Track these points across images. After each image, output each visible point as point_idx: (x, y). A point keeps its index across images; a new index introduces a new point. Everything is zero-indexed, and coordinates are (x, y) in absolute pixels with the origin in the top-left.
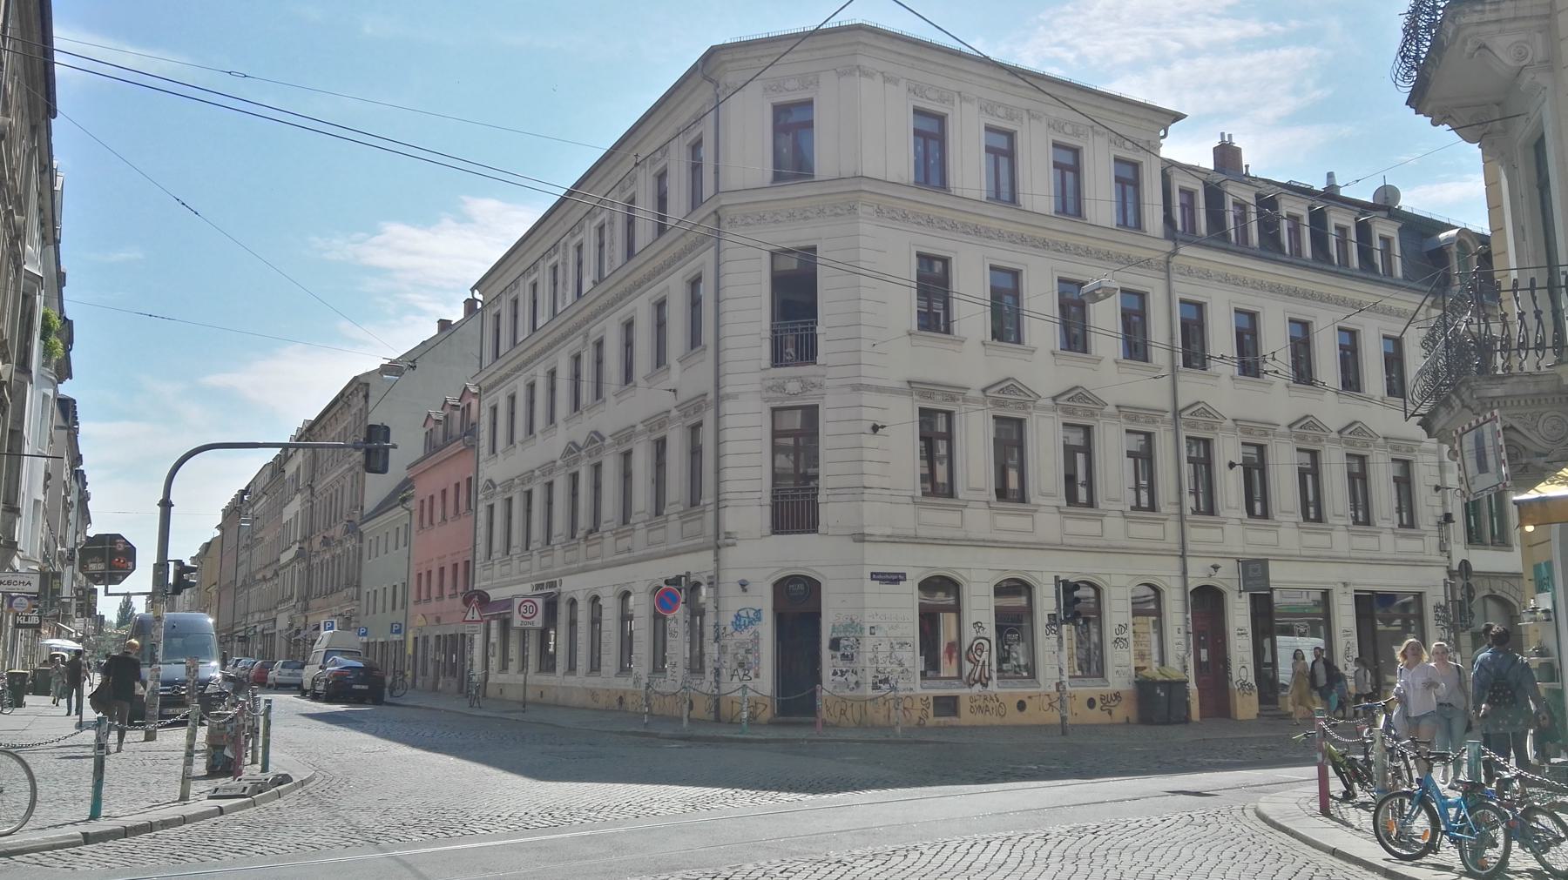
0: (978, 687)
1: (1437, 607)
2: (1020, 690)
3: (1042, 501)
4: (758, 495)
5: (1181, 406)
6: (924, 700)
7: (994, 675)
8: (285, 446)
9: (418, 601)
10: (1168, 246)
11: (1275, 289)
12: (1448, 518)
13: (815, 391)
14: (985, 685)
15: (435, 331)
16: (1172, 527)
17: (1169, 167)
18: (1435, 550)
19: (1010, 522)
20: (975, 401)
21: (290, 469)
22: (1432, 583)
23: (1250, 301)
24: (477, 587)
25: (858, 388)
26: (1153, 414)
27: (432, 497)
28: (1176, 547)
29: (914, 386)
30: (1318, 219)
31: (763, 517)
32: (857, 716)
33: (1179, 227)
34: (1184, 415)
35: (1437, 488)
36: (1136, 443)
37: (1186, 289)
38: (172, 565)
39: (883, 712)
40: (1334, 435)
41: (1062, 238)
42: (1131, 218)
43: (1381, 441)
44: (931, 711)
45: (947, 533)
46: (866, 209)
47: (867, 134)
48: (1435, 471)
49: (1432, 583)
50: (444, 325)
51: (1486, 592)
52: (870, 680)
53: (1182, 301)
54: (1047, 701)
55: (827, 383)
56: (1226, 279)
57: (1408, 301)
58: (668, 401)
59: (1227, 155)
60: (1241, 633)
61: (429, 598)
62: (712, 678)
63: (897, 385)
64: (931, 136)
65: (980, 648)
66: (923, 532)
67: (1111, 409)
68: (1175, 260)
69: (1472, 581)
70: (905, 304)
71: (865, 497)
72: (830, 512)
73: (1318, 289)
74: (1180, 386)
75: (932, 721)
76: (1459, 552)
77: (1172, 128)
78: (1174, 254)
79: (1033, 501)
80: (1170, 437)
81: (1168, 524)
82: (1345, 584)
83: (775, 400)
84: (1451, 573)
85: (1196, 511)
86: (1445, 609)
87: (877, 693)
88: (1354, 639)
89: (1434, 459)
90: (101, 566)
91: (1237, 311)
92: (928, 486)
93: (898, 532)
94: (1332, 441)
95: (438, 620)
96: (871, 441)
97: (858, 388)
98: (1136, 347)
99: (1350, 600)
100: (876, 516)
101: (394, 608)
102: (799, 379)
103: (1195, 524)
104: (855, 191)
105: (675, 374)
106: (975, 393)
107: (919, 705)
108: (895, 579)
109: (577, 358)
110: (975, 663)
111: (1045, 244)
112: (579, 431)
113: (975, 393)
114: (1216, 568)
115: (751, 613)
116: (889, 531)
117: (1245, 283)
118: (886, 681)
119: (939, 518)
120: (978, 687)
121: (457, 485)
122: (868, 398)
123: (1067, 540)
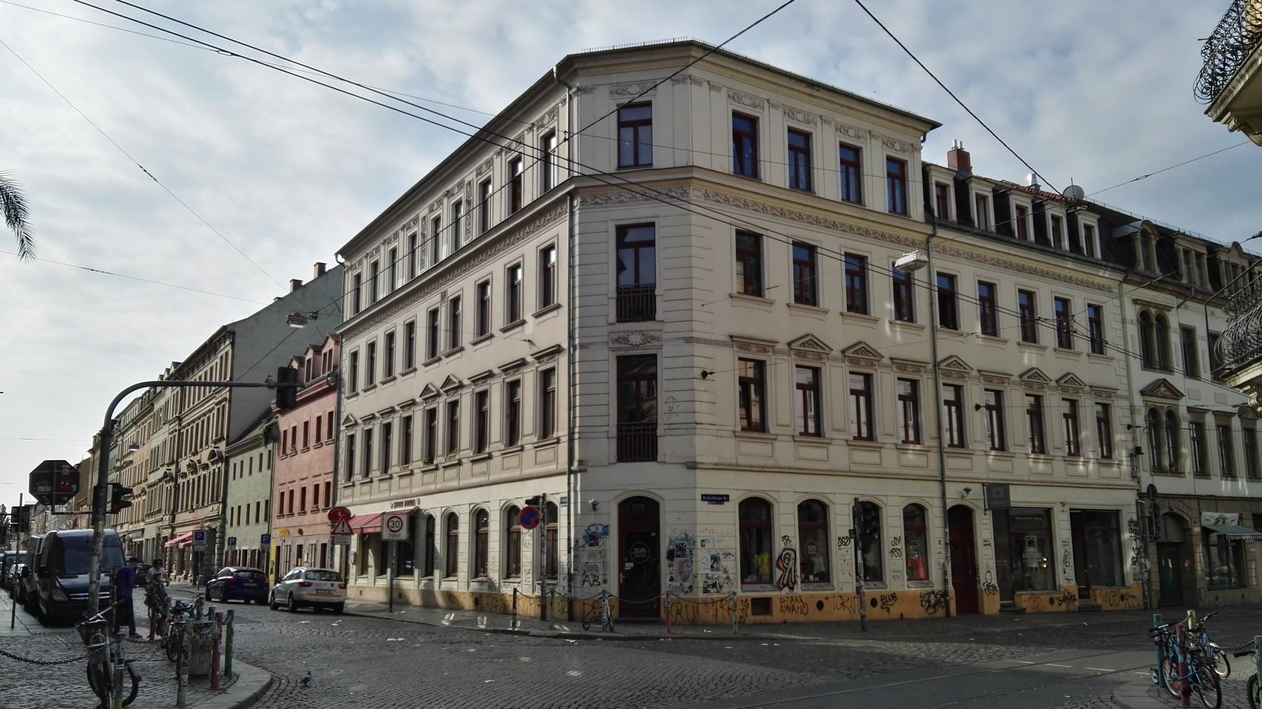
0: (786, 590)
1: (1131, 522)
2: (820, 593)
3: (780, 431)
4: (606, 429)
5: (939, 358)
6: (744, 601)
7: (799, 580)
8: (153, 385)
9: (281, 515)
10: (928, 229)
11: (1008, 266)
12: (1138, 451)
13: (654, 343)
14: (792, 589)
15: (1230, 245)
16: (934, 456)
17: (926, 168)
18: (1128, 478)
19: (812, 454)
20: (782, 352)
21: (159, 404)
22: (1126, 502)
23: (989, 275)
24: (338, 504)
25: (689, 340)
26: (918, 366)
27: (294, 428)
28: (937, 473)
29: (736, 341)
30: (1038, 208)
31: (610, 448)
32: (691, 617)
33: (936, 214)
34: (943, 366)
35: (1129, 427)
36: (904, 389)
37: (941, 264)
38: (110, 487)
39: (711, 612)
40: (1053, 384)
41: (849, 221)
42: (899, 206)
43: (1087, 388)
44: (749, 611)
45: (761, 462)
46: (696, 192)
47: (693, 129)
48: (1127, 413)
49: (1126, 502)
50: (297, 284)
51: (1166, 510)
52: (701, 584)
53: (939, 274)
54: (840, 601)
55: (664, 336)
56: (971, 257)
57: (1105, 276)
58: (525, 352)
59: (962, 157)
60: (986, 544)
61: (291, 513)
62: (565, 583)
63: (722, 339)
64: (745, 133)
65: (788, 557)
66: (742, 461)
67: (886, 361)
68: (934, 241)
69: (1157, 501)
70: (728, 272)
71: (697, 431)
72: (666, 445)
73: (1039, 266)
74: (938, 343)
75: (751, 618)
76: (1146, 479)
77: (930, 134)
78: (934, 235)
79: (827, 435)
80: (931, 383)
81: (930, 454)
82: (1063, 504)
83: (620, 349)
84: (1140, 495)
85: (951, 445)
86: (1136, 524)
87: (706, 595)
88: (1070, 548)
89: (1126, 403)
90: (48, 489)
91: (980, 283)
92: (745, 423)
93: (724, 461)
94: (1051, 388)
95: (301, 532)
96: (700, 384)
97: (689, 340)
98: (904, 310)
99: (1067, 516)
100: (705, 447)
101: (257, 521)
102: (642, 332)
103: (951, 455)
104: (679, 182)
105: (531, 327)
106: (782, 346)
107: (740, 606)
108: (721, 499)
109: (434, 314)
110: (784, 569)
111: (834, 225)
112: (434, 375)
113: (782, 346)
114: (967, 491)
115: (600, 529)
116: (715, 460)
117: (985, 261)
118: (714, 585)
119: (754, 450)
120: (786, 590)
121: (319, 419)
122: (698, 349)
123: (854, 468)
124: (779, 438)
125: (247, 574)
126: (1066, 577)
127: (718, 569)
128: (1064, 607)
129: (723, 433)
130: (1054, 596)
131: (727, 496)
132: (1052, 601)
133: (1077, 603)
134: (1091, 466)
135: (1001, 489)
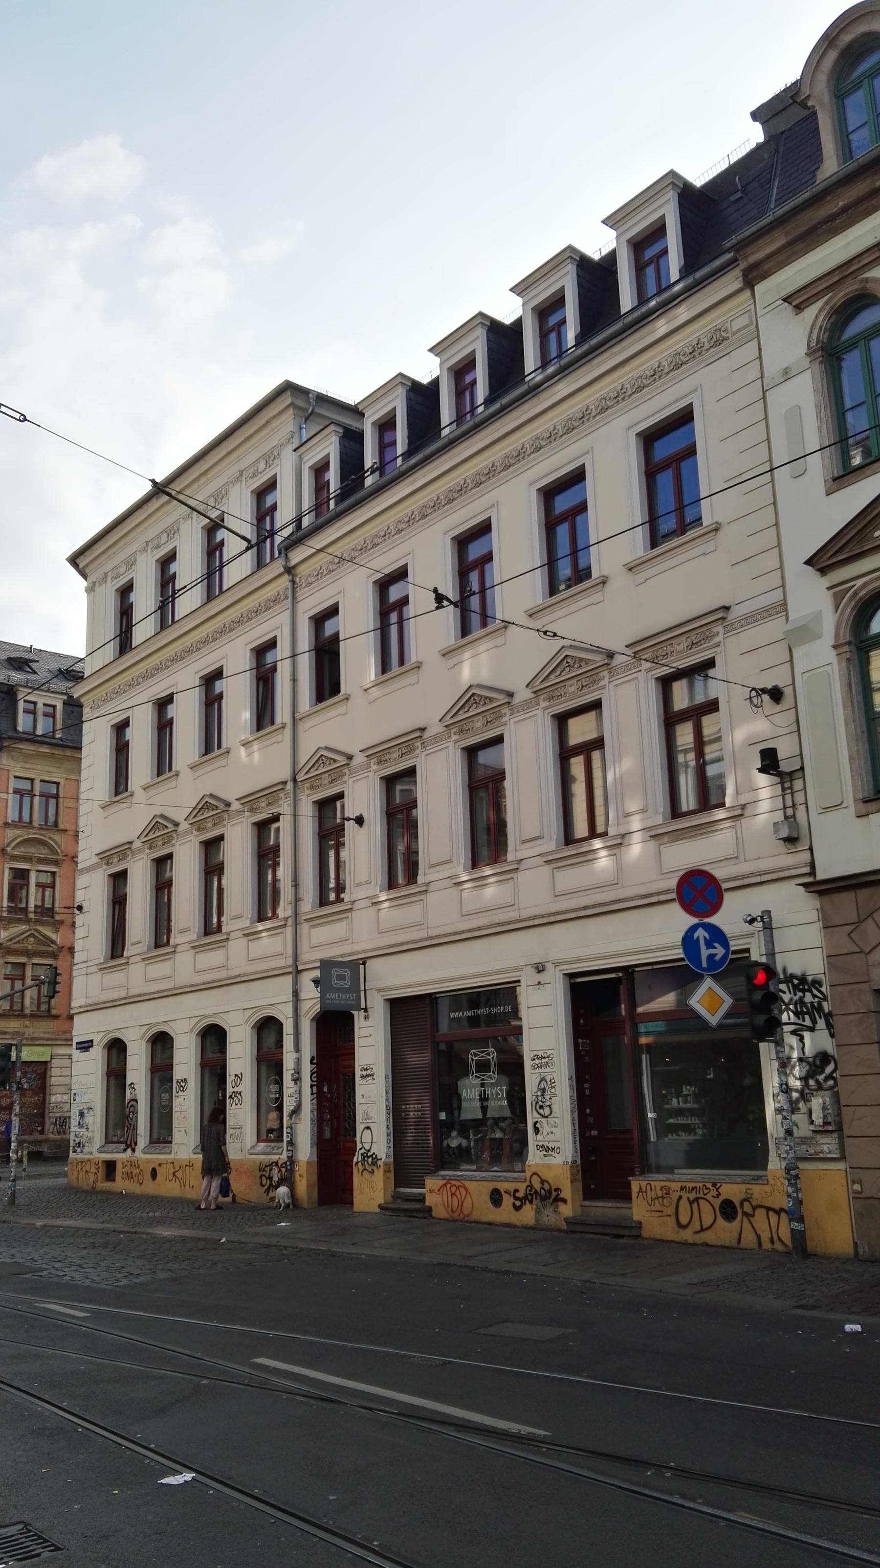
82: (540, 969)
124: (432, 887)
125: (462, 1168)
126: (554, 1142)
127: (83, 1127)
128: (528, 1215)
129: (90, 970)
130: (502, 1186)
131: (92, 1041)
132: (496, 1198)
133: (566, 1210)
134: (636, 849)
135: (347, 973)
